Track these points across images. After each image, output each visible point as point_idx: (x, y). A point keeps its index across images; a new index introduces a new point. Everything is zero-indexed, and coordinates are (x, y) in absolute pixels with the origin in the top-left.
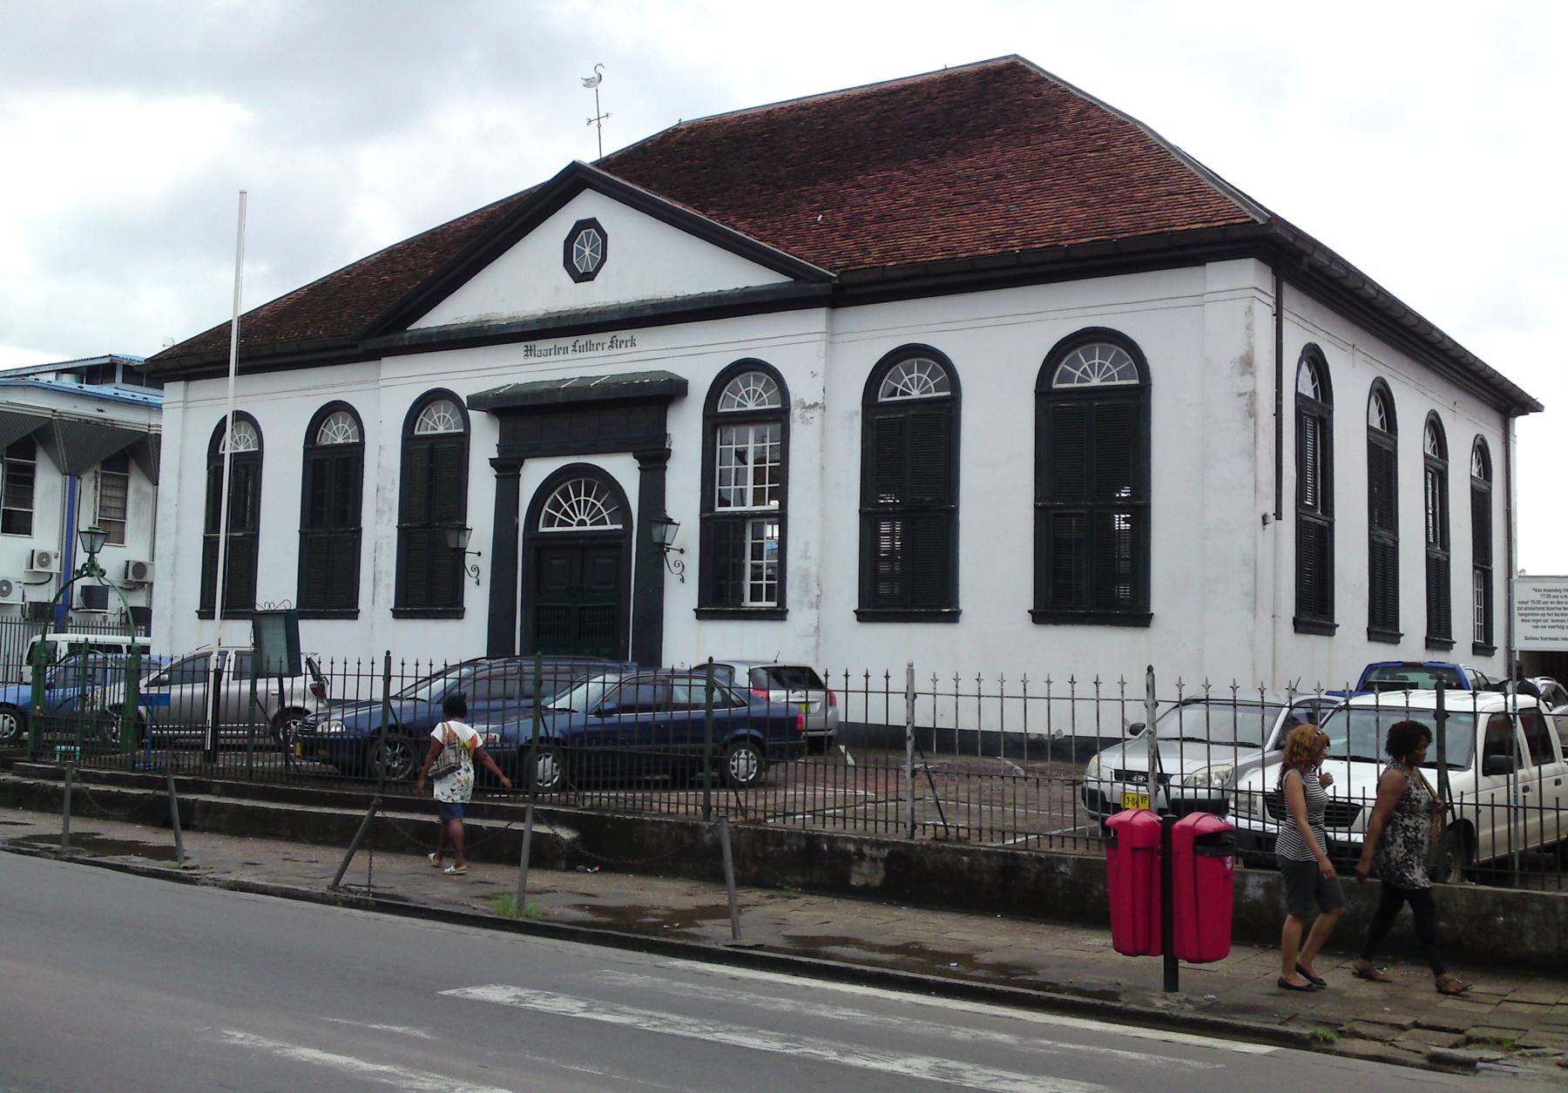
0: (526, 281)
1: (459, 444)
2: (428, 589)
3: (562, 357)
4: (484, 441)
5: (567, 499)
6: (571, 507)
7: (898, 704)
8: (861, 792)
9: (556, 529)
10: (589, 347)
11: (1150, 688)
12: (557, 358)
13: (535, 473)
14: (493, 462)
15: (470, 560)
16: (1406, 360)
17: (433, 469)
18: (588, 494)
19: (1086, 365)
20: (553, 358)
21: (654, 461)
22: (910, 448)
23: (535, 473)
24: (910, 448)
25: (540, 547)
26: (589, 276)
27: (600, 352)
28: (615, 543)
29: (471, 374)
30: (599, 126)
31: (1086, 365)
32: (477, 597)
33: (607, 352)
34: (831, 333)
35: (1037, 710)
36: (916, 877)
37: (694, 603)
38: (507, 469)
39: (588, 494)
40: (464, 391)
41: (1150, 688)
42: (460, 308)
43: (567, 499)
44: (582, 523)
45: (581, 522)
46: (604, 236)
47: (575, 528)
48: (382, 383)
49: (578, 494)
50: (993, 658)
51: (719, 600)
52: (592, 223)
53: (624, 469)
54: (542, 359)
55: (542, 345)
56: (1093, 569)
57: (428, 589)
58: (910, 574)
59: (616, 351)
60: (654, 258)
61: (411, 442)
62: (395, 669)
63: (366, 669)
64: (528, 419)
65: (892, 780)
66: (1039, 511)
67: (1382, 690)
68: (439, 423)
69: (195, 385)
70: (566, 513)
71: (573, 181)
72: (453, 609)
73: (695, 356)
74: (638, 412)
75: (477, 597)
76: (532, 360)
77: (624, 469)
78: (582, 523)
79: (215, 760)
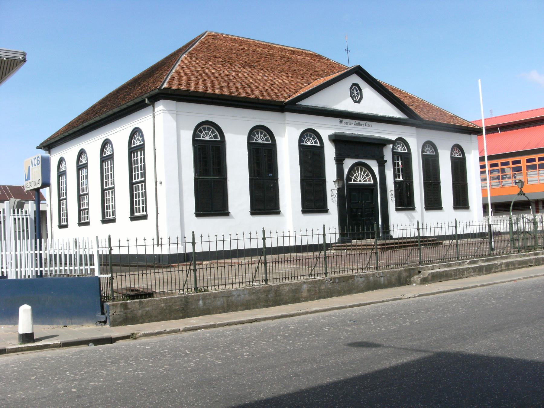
3: (351, 126)
4: (330, 152)
7: (261, 242)
8: (295, 266)
10: (360, 125)
11: (193, 239)
12: (350, 126)
18: (358, 172)
20: (348, 126)
21: (382, 164)
22: (263, 158)
23: (348, 163)
24: (263, 158)
26: (358, 102)
27: (362, 127)
28: (371, 189)
29: (327, 129)
33: (364, 127)
35: (247, 242)
38: (339, 161)
39: (361, 172)
41: (193, 239)
45: (361, 179)
47: (358, 182)
48: (286, 122)
49: (361, 172)
52: (357, 85)
53: (374, 165)
54: (345, 125)
55: (345, 120)
57: (313, 202)
58: (265, 201)
59: (367, 128)
62: (327, 231)
63: (315, 232)
64: (345, 145)
66: (453, 184)
72: (322, 209)
74: (373, 148)
75: (332, 204)
76: (342, 125)
78: (360, 181)
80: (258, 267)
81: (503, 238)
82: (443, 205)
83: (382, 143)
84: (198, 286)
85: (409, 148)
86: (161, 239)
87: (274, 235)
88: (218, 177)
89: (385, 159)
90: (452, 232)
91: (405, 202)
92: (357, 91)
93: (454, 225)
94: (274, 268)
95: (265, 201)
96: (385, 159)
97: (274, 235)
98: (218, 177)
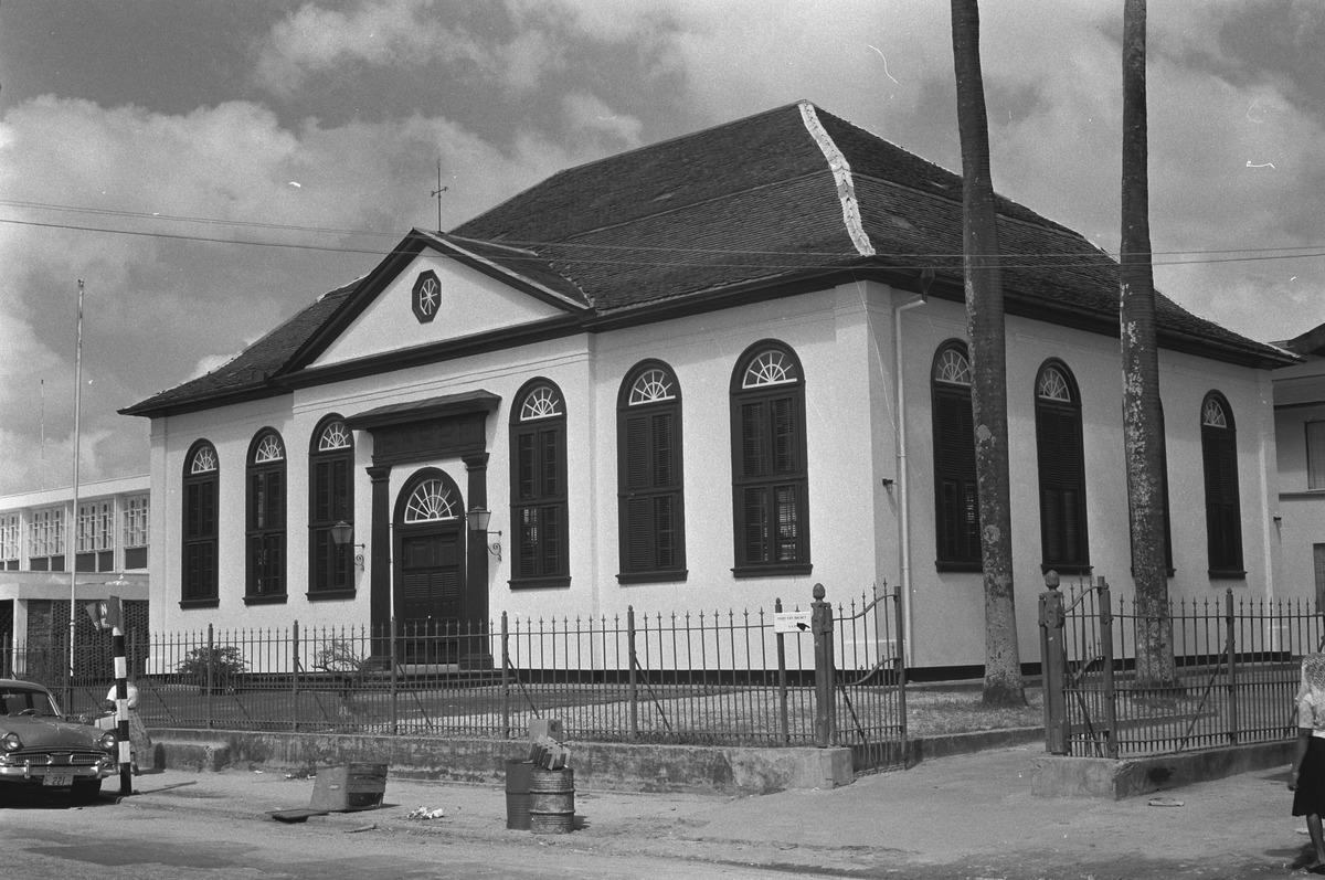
0: (386, 325)
1: (345, 460)
2: (331, 579)
5: (422, 497)
6: (426, 503)
9: (416, 521)
13: (399, 477)
14: (369, 470)
15: (491, 539)
16: (1096, 336)
17: (330, 480)
19: (759, 376)
21: (477, 465)
22: (650, 446)
23: (399, 477)
24: (650, 446)
25: (408, 537)
30: (440, 197)
31: (759, 376)
32: (364, 583)
34: (593, 351)
36: (227, 814)
37: (615, 568)
38: (379, 477)
39: (436, 493)
40: (347, 413)
42: (338, 353)
43: (422, 497)
44: (433, 516)
45: (434, 512)
46: (439, 283)
47: (428, 520)
48: (837, 312)
50: (717, 610)
51: (523, 579)
53: (456, 470)
56: (771, 538)
57: (331, 579)
58: (652, 548)
60: (476, 303)
61: (314, 453)
64: (398, 433)
65: (732, 708)
67: (282, 678)
68: (335, 442)
69: (170, 419)
70: (422, 509)
71: (415, 244)
73: (501, 378)
75: (364, 583)
77: (456, 470)
78: (433, 516)
79: (93, 724)
80: (1192, 727)
81: (473, 693)
82: (692, 563)
83: (479, 409)
84: (791, 731)
85: (562, 406)
86: (492, 624)
87: (653, 624)
88: (391, 521)
89: (487, 451)
90: (614, 658)
91: (543, 562)
92: (424, 302)
93: (291, 636)
94: (1167, 731)
95: (652, 548)
96: (487, 451)
97: (653, 624)
98: (391, 521)
